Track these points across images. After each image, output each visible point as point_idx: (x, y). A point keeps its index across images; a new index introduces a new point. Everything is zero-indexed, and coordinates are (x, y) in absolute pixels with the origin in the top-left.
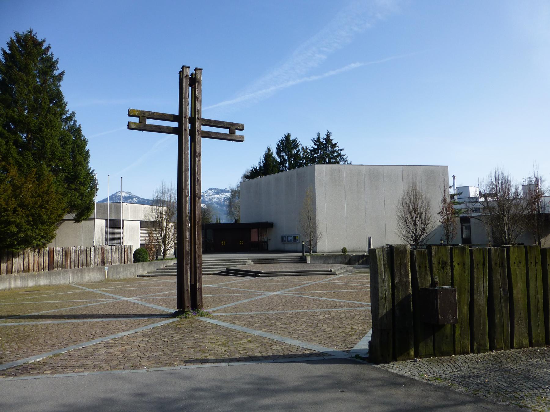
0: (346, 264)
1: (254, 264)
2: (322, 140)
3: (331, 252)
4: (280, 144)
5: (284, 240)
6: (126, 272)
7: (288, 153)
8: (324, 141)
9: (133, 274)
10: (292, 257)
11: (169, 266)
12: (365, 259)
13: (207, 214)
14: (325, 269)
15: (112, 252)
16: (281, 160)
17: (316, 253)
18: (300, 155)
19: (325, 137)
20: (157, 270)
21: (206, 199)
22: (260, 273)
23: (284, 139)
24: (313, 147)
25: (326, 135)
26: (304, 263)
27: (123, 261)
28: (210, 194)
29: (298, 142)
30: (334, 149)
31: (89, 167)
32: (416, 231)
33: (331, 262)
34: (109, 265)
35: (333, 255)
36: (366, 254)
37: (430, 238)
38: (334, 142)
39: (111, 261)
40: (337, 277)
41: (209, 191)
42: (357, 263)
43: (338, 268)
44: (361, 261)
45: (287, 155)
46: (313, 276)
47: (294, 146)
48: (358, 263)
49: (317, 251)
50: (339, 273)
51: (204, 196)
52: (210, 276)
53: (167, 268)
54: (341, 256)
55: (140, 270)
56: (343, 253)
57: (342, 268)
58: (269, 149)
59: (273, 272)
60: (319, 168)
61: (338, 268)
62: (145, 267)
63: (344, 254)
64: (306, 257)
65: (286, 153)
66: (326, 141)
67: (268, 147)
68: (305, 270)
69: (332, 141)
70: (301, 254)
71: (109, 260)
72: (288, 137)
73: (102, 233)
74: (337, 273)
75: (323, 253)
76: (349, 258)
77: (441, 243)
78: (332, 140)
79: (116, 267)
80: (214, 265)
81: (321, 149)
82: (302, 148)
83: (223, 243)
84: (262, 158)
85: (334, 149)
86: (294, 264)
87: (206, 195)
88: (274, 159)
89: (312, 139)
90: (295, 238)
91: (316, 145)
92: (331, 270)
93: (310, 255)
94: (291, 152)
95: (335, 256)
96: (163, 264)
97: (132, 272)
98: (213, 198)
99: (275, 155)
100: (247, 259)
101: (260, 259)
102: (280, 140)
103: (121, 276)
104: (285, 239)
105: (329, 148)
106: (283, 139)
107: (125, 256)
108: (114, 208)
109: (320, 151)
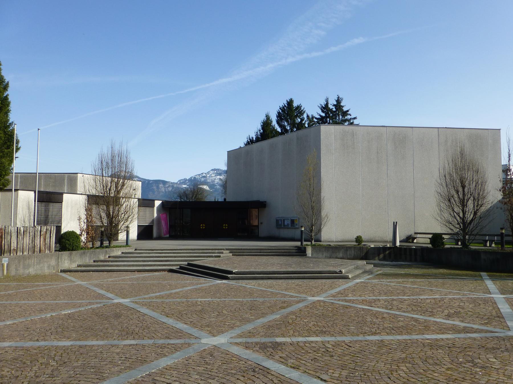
0: (362, 259)
1: (232, 255)
2: (331, 106)
3: (340, 242)
4: (280, 111)
5: (280, 224)
6: (42, 265)
7: (291, 121)
8: (334, 107)
9: (54, 268)
10: (286, 247)
11: (114, 257)
12: (387, 252)
13: (200, 193)
14: (331, 269)
15: (18, 236)
16: (281, 130)
17: (321, 241)
18: (304, 124)
19: (335, 103)
20: (94, 261)
21: (209, 181)
22: (231, 273)
23: (286, 105)
24: (320, 115)
25: (336, 101)
26: (302, 257)
27: (37, 249)
28: (213, 175)
29: (302, 109)
30: (346, 118)
31: (10, 121)
32: (464, 213)
33: (341, 255)
34: (12, 255)
35: (344, 245)
36: (388, 246)
37: (485, 226)
38: (345, 109)
39: (16, 249)
40: (351, 284)
41: (212, 172)
42: (377, 258)
43: (351, 267)
44: (381, 256)
45: (288, 124)
46: (313, 280)
47: (298, 114)
48: (379, 258)
49: (322, 240)
50: (353, 276)
51: (206, 177)
52: (164, 273)
53: (110, 259)
54: (354, 247)
55: (66, 262)
56: (357, 244)
57: (357, 268)
58: (268, 117)
59: (250, 272)
60: (324, 128)
61: (351, 267)
62: (74, 258)
63: (358, 245)
64: (305, 248)
65: (288, 122)
66: (336, 108)
67: (266, 115)
68: (301, 270)
69: (343, 108)
70: (298, 244)
71: (12, 248)
72: (290, 103)
73: (29, 209)
74: (350, 277)
75: (329, 242)
76: (365, 251)
77: (501, 233)
78: (343, 107)
79: (24, 258)
80: (175, 257)
81: (329, 117)
82: (308, 116)
83: (202, 226)
84: (260, 127)
85: (346, 118)
86: (288, 258)
87: (208, 176)
88: (274, 128)
89: (320, 106)
90: (293, 221)
91: (323, 113)
92: (340, 271)
93: (312, 245)
94: (294, 121)
95: (346, 247)
96: (104, 254)
97: (52, 264)
98: (215, 179)
99: (274, 123)
100: (224, 249)
101: (241, 249)
102: (281, 106)
103: (32, 271)
104: (280, 223)
105: (339, 116)
106: (285, 105)
107: (41, 242)
108: (67, 180)
109: (328, 119)
